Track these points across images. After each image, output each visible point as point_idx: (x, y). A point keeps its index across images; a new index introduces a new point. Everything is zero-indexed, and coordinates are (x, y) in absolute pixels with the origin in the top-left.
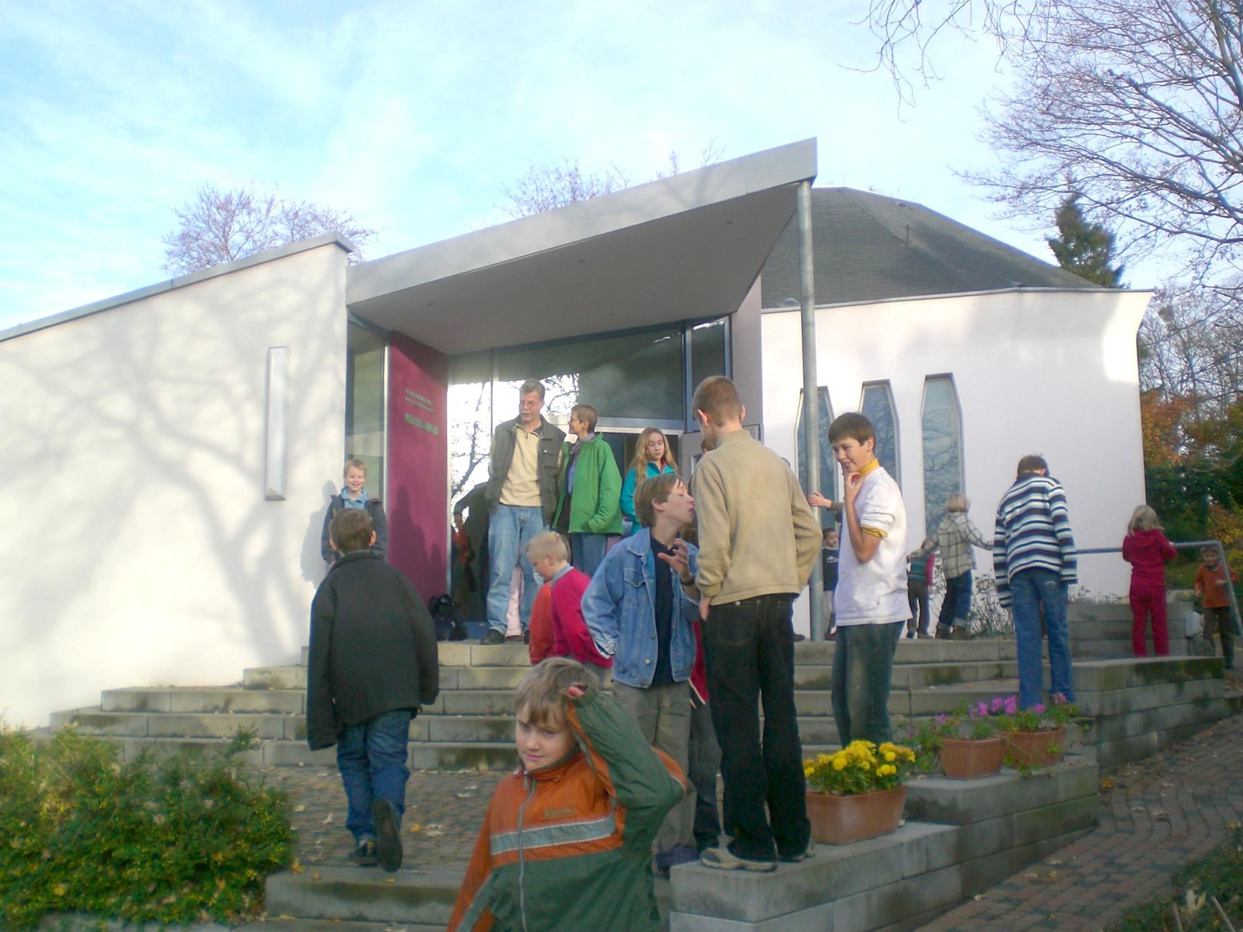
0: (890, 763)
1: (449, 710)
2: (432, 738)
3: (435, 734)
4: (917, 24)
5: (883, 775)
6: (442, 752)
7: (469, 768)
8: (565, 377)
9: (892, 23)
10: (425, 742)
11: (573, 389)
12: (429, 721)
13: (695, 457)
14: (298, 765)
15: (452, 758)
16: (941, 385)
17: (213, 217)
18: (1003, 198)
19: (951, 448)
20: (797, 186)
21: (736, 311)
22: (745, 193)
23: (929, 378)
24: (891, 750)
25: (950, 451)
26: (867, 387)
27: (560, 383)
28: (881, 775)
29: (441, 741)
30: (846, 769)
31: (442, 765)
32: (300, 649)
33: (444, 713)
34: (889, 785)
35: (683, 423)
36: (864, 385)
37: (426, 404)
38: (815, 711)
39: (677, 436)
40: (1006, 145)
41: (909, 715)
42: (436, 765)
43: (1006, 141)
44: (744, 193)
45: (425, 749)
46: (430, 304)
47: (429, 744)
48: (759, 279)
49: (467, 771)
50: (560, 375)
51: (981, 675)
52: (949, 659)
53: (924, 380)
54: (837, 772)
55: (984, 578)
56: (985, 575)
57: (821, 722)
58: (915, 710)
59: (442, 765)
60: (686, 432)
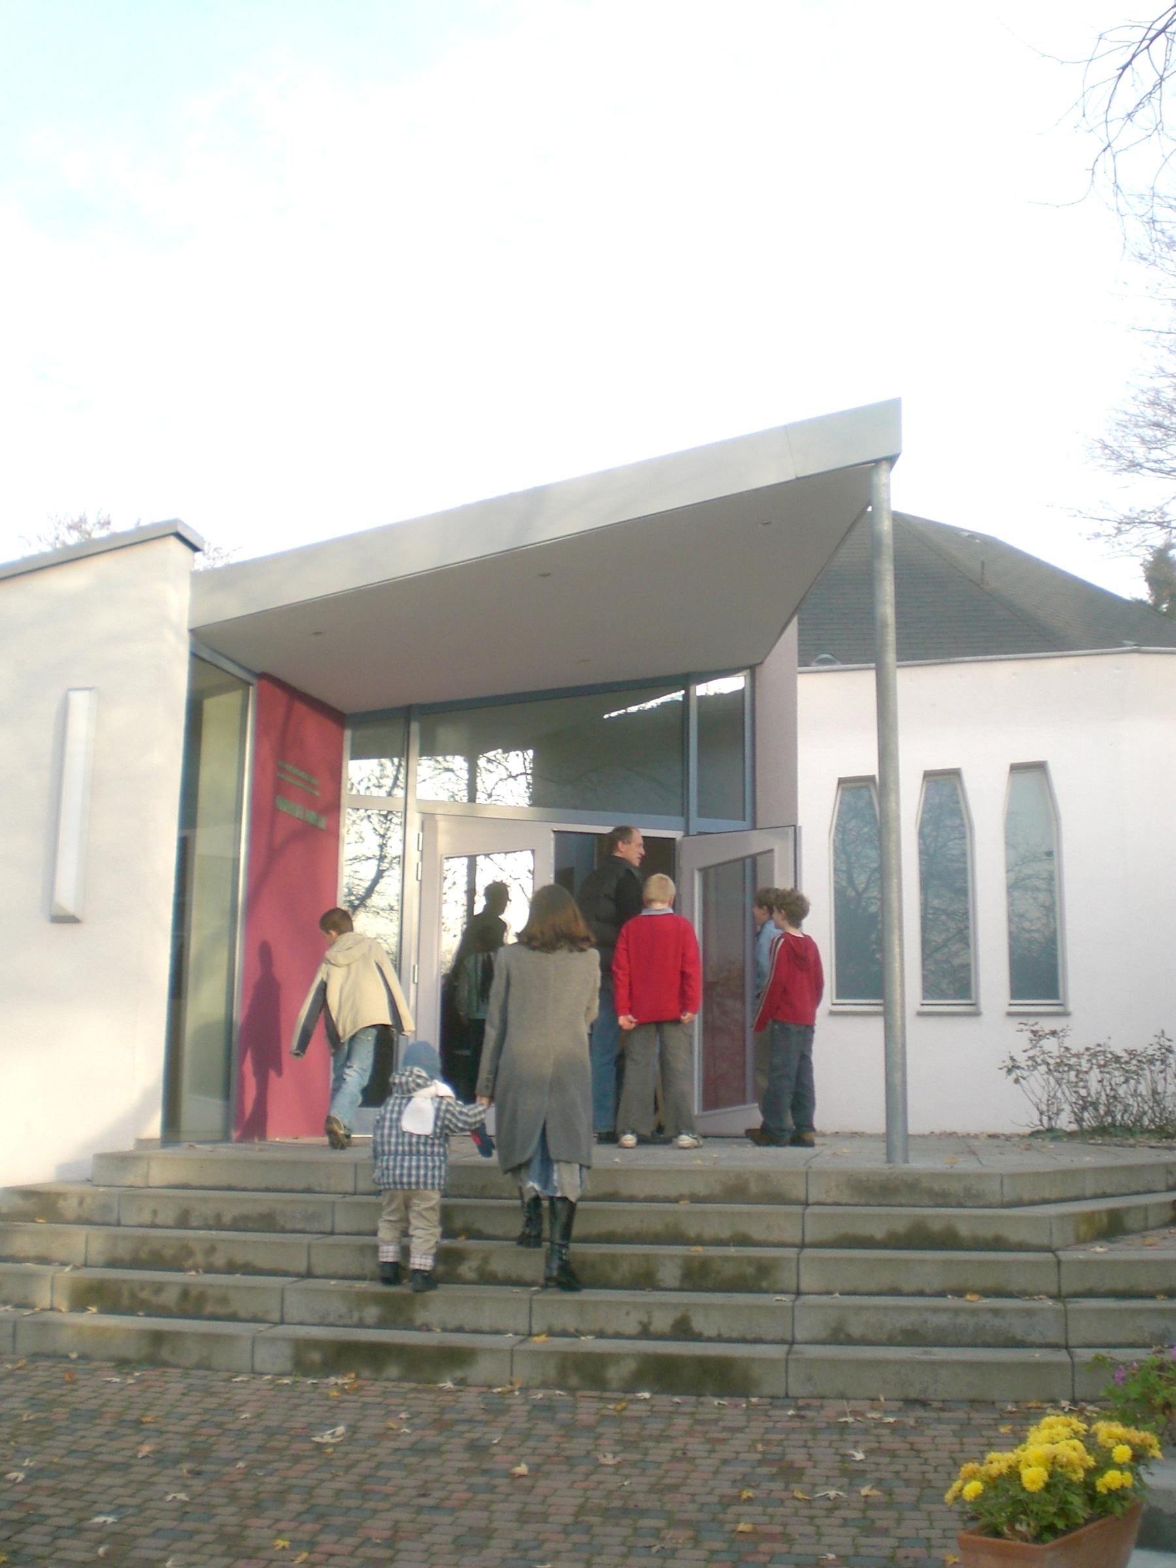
0: (1120, 1467)
1: (318, 1271)
2: (287, 1318)
3: (293, 1313)
4: (1158, 121)
5: (1109, 1490)
6: (302, 1346)
7: (344, 1375)
8: (513, 754)
9: (1111, 121)
10: (276, 1324)
11: (524, 771)
12: (283, 1291)
13: (700, 870)
14: (67, 1357)
15: (316, 1356)
16: (1031, 777)
17: (61, 538)
18: (1098, 535)
19: (1017, 865)
20: (872, 468)
21: (761, 663)
22: (793, 477)
23: (1016, 768)
24: (1121, 1441)
25: (1017, 869)
26: (844, 785)
27: (505, 764)
28: (1105, 1491)
29: (301, 1323)
30: (1048, 1487)
31: (301, 1366)
32: (91, 1156)
33: (309, 1274)
34: (1118, 1510)
35: (680, 820)
36: (842, 782)
37: (299, 778)
38: (906, 1287)
39: (673, 839)
40: (1102, 466)
41: (1057, 1296)
42: (288, 1366)
43: (1103, 462)
44: (792, 477)
45: (273, 1340)
46: (316, 633)
47: (281, 1330)
48: (795, 620)
49: (340, 1381)
50: (506, 750)
51: (1152, 1222)
52: (1099, 1191)
53: (1008, 769)
54: (1031, 1494)
55: (1099, 1049)
56: (1099, 1045)
57: (919, 1310)
58: (1067, 1287)
59: (301, 1366)
60: (687, 834)
